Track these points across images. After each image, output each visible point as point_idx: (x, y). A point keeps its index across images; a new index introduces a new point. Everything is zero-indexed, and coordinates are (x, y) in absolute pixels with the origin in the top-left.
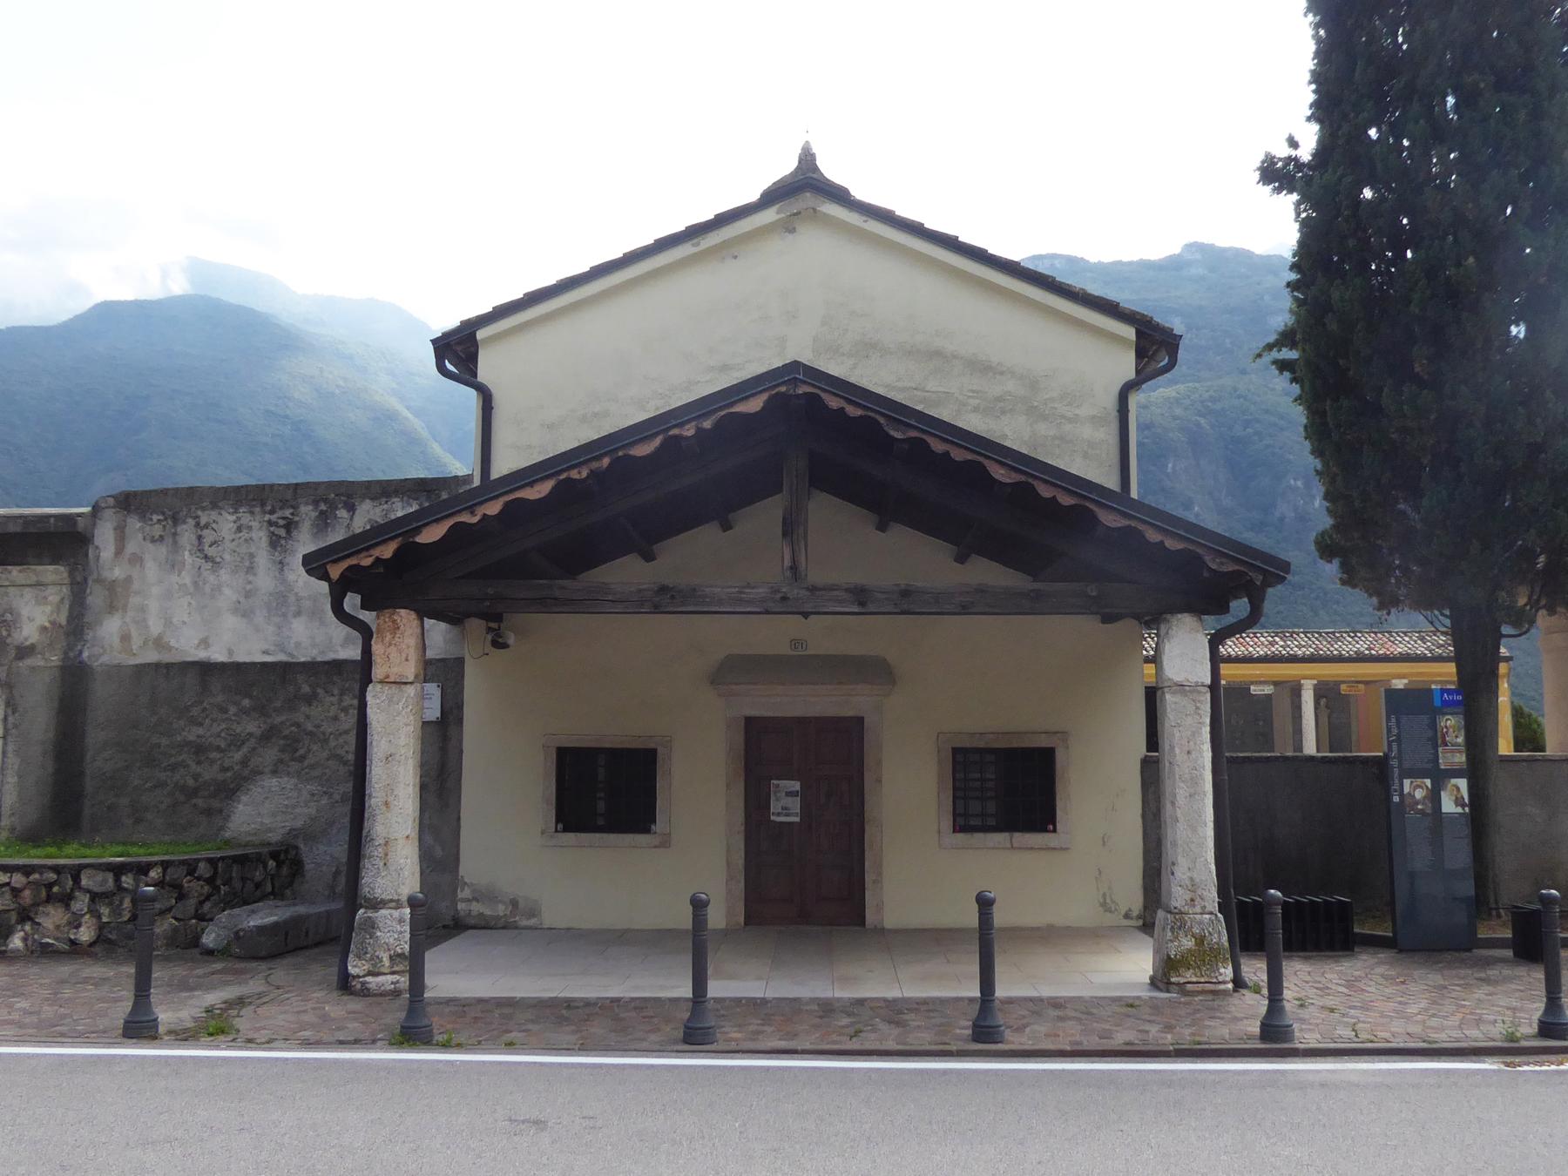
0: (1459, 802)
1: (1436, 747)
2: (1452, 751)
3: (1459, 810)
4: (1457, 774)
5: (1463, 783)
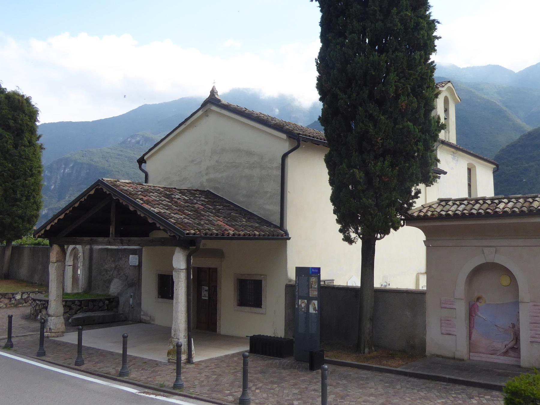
0: (315, 309)
1: (309, 289)
2: (314, 291)
3: (314, 312)
4: (315, 299)
5: (316, 302)
